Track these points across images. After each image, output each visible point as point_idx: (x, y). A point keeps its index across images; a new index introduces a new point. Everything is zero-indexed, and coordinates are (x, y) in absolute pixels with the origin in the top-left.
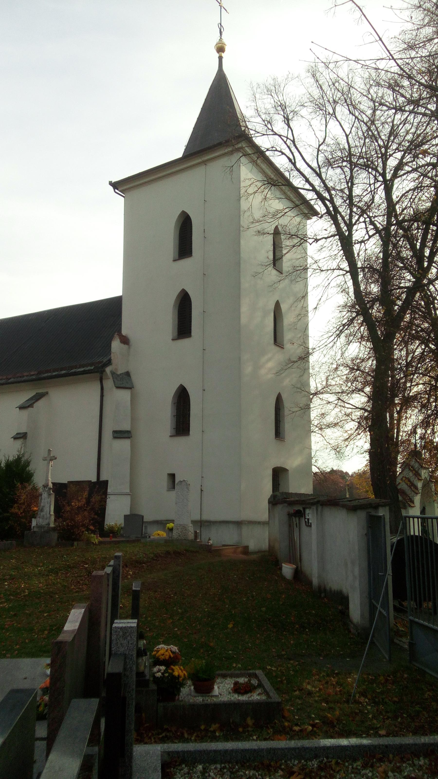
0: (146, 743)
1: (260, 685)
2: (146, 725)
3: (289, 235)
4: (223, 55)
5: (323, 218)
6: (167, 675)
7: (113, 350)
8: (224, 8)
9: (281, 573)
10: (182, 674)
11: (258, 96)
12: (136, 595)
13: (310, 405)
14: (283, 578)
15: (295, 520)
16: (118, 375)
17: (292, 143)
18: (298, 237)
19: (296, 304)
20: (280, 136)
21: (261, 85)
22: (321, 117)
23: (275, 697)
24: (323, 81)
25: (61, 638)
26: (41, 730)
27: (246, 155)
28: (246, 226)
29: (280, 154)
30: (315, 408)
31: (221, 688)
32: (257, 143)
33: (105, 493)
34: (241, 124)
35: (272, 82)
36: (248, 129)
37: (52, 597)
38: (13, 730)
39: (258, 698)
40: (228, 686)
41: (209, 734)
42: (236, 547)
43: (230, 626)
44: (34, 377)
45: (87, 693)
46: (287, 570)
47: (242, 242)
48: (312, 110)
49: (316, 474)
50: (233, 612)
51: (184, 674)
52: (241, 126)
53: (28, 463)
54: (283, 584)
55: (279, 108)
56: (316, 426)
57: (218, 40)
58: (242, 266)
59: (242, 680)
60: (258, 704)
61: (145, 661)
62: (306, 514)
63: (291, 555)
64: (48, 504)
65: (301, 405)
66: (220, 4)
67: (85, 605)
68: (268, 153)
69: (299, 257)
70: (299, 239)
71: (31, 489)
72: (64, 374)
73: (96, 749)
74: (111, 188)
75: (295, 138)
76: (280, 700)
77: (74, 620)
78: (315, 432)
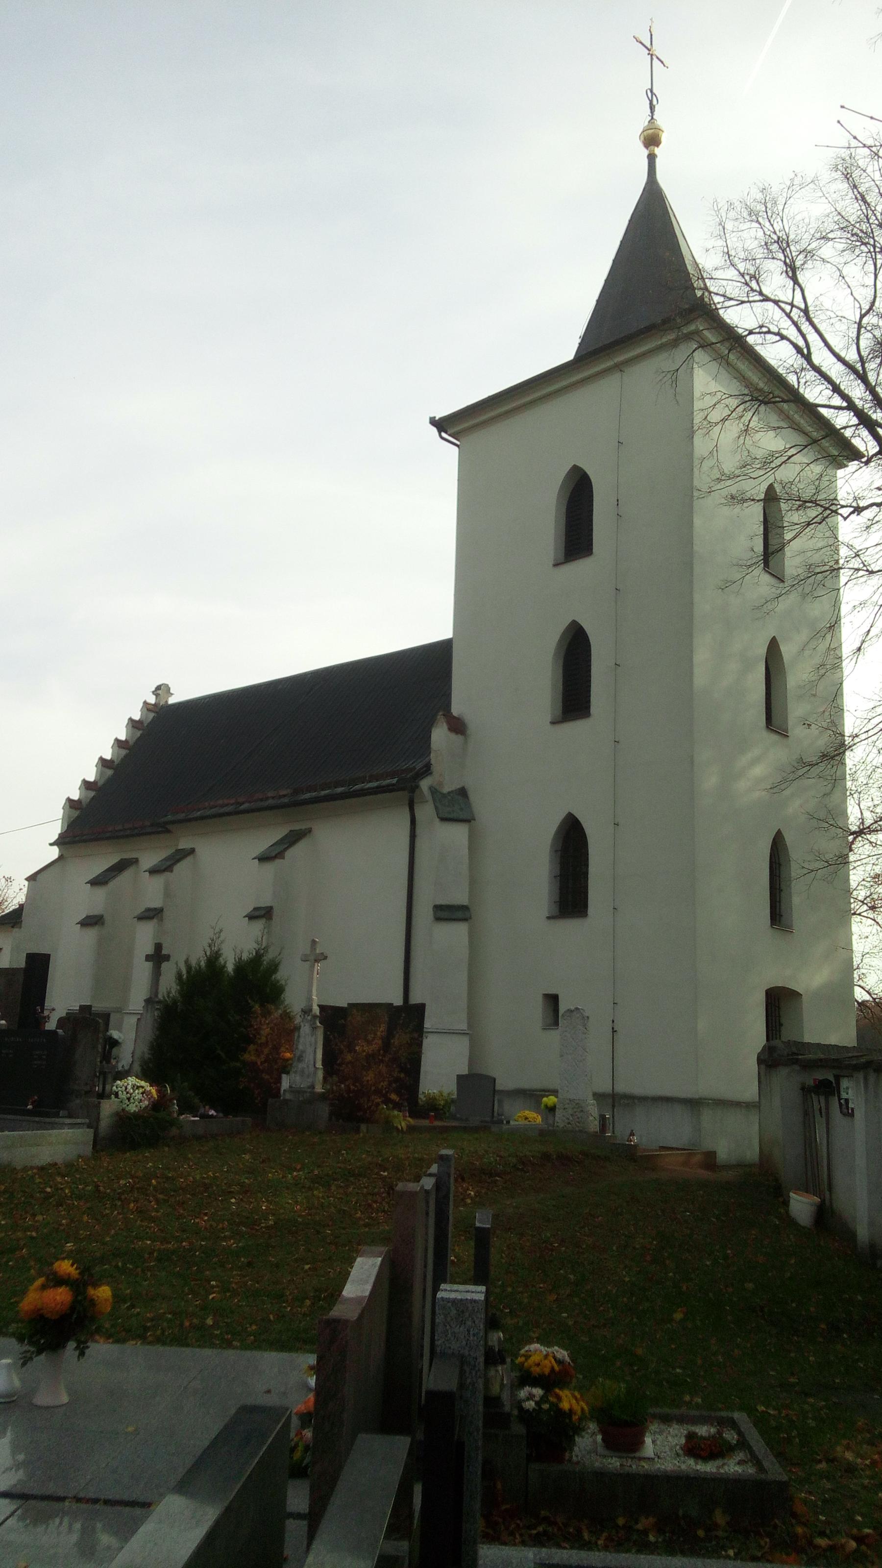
0: (505, 1544)
1: (743, 1444)
2: (504, 1507)
3: (797, 503)
4: (657, 151)
5: (872, 464)
6: (546, 1406)
7: (434, 746)
8: (658, 58)
9: (787, 1212)
10: (577, 1408)
11: (729, 226)
12: (482, 1238)
13: (848, 857)
14: (791, 1222)
15: (818, 1102)
16: (444, 796)
17: (802, 314)
18: (819, 505)
19: (812, 645)
20: (776, 302)
21: (737, 204)
22: (864, 259)
23: (775, 1471)
24: (867, 185)
25: (337, 1311)
26: (298, 1498)
27: (704, 345)
28: (705, 488)
29: (778, 338)
30: (859, 863)
31: (658, 1442)
32: (728, 321)
33: (419, 1029)
34: (695, 286)
35: (759, 196)
36: (710, 292)
37: (318, 1232)
38: (244, 1487)
39: (739, 1469)
40: (673, 1441)
41: (635, 1537)
42: (688, 1152)
43: (678, 1316)
44: (286, 800)
45: (389, 1422)
46: (801, 1206)
47: (697, 521)
48: (846, 245)
49: (862, 1004)
50: (685, 1288)
51: (582, 1409)
52: (694, 289)
53: (274, 967)
54: (791, 1236)
55: (775, 247)
56: (862, 902)
57: (646, 123)
58: (697, 569)
59: (703, 1431)
60: (737, 1482)
61: (502, 1374)
62: (842, 1090)
63: (809, 1174)
64: (311, 1046)
65: (828, 857)
66: (649, 50)
67: (384, 1249)
68: (751, 339)
69: (820, 545)
70: (820, 509)
71: (281, 1015)
72: (341, 793)
73: (405, 1545)
74: (434, 430)
75: (809, 304)
76: (785, 1478)
77: (362, 1277)
78: (859, 914)
